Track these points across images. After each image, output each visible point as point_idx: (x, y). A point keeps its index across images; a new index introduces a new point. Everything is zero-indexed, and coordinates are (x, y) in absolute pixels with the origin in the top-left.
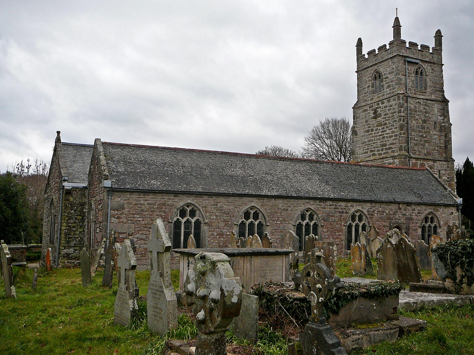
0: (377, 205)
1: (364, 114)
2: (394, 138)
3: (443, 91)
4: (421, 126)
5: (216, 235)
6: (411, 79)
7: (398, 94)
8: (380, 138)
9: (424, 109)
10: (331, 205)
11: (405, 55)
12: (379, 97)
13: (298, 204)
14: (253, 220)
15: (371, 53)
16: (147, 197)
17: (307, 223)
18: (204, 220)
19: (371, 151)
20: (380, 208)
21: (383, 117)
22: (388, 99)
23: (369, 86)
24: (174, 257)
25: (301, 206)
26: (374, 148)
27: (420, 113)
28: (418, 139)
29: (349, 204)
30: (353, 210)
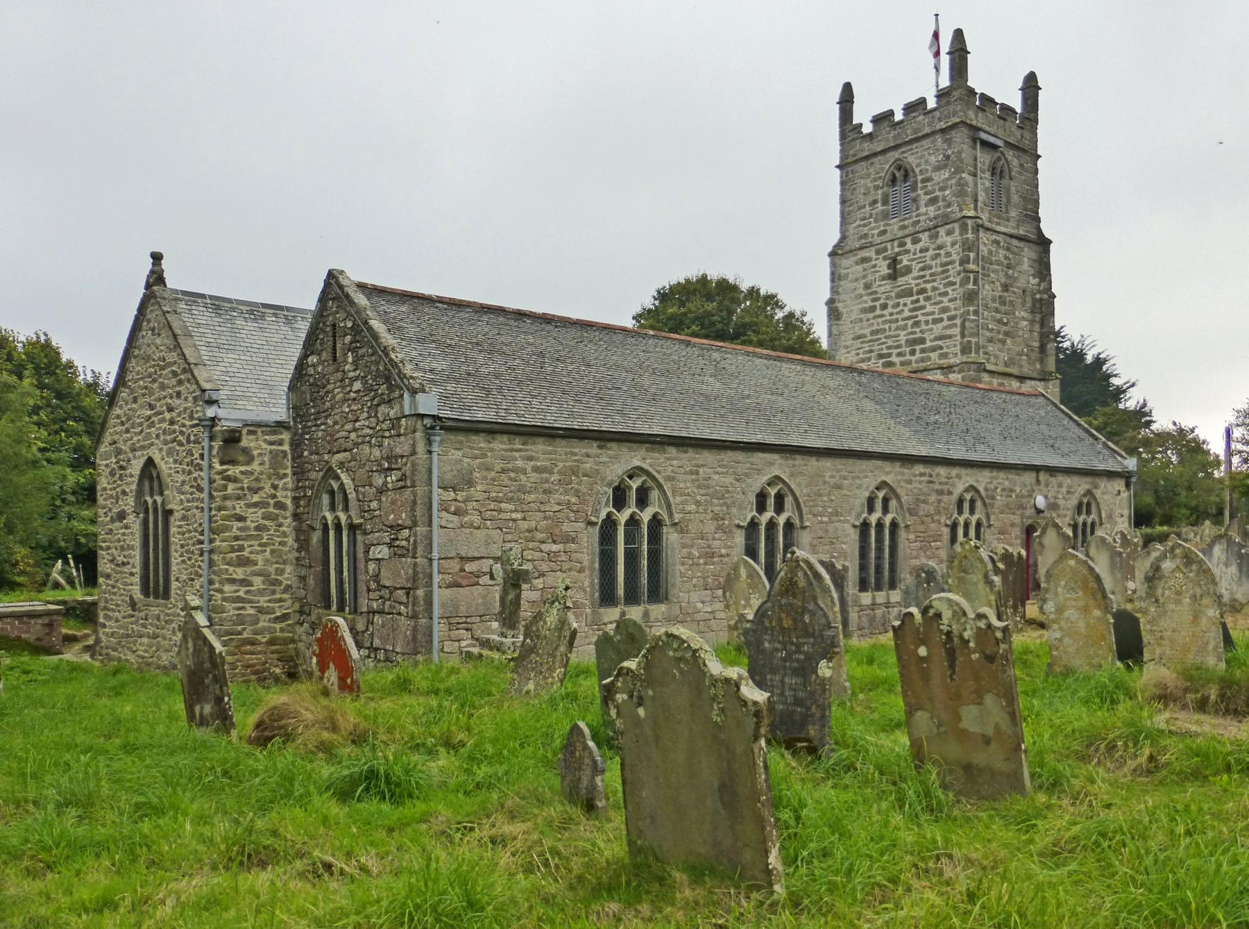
1: (860, 268)
2: (946, 323)
3: (1038, 220)
4: (1000, 297)
5: (699, 558)
7: (964, 217)
8: (906, 325)
9: (1006, 258)
11: (974, 123)
12: (903, 227)
13: (861, 471)
14: (615, 511)
15: (883, 119)
16: (533, 447)
17: (771, 519)
18: (671, 515)
19: (881, 356)
21: (915, 273)
22: (933, 230)
23: (875, 202)
24: (605, 624)
25: (870, 476)
26: (889, 348)
30: (960, 487)
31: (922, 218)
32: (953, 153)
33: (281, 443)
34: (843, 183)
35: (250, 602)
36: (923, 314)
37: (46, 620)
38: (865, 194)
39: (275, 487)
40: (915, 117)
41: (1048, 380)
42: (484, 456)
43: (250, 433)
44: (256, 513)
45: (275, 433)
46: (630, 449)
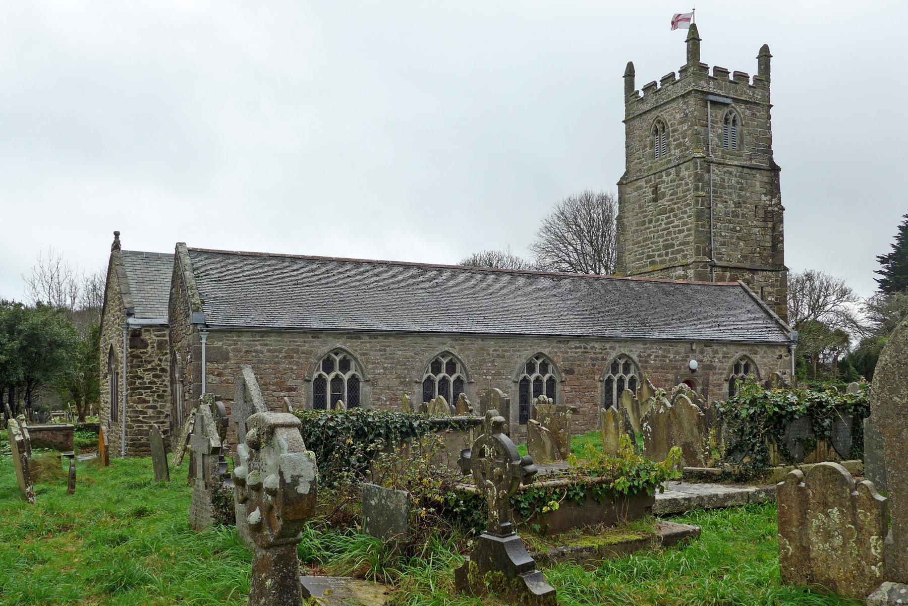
0: (655, 346)
3: (771, 153)
5: (386, 401)
6: (717, 131)
7: (694, 157)
8: (663, 234)
10: (576, 348)
18: (363, 375)
20: (656, 351)
23: (645, 146)
26: (653, 251)
27: (730, 191)
28: (727, 234)
29: (608, 346)
30: (613, 355)
31: (672, 158)
32: (689, 112)
33: (164, 336)
34: (627, 134)
35: (146, 423)
36: (673, 227)
37: (65, 432)
38: (639, 141)
39: (160, 360)
40: (667, 87)
41: (778, 271)
42: (236, 344)
43: (146, 331)
44: (149, 374)
45: (160, 330)
46: (334, 338)
